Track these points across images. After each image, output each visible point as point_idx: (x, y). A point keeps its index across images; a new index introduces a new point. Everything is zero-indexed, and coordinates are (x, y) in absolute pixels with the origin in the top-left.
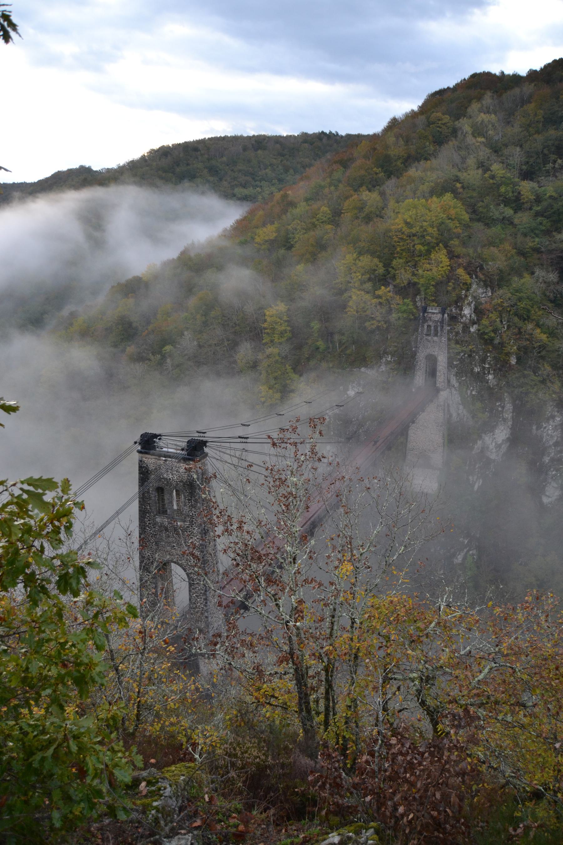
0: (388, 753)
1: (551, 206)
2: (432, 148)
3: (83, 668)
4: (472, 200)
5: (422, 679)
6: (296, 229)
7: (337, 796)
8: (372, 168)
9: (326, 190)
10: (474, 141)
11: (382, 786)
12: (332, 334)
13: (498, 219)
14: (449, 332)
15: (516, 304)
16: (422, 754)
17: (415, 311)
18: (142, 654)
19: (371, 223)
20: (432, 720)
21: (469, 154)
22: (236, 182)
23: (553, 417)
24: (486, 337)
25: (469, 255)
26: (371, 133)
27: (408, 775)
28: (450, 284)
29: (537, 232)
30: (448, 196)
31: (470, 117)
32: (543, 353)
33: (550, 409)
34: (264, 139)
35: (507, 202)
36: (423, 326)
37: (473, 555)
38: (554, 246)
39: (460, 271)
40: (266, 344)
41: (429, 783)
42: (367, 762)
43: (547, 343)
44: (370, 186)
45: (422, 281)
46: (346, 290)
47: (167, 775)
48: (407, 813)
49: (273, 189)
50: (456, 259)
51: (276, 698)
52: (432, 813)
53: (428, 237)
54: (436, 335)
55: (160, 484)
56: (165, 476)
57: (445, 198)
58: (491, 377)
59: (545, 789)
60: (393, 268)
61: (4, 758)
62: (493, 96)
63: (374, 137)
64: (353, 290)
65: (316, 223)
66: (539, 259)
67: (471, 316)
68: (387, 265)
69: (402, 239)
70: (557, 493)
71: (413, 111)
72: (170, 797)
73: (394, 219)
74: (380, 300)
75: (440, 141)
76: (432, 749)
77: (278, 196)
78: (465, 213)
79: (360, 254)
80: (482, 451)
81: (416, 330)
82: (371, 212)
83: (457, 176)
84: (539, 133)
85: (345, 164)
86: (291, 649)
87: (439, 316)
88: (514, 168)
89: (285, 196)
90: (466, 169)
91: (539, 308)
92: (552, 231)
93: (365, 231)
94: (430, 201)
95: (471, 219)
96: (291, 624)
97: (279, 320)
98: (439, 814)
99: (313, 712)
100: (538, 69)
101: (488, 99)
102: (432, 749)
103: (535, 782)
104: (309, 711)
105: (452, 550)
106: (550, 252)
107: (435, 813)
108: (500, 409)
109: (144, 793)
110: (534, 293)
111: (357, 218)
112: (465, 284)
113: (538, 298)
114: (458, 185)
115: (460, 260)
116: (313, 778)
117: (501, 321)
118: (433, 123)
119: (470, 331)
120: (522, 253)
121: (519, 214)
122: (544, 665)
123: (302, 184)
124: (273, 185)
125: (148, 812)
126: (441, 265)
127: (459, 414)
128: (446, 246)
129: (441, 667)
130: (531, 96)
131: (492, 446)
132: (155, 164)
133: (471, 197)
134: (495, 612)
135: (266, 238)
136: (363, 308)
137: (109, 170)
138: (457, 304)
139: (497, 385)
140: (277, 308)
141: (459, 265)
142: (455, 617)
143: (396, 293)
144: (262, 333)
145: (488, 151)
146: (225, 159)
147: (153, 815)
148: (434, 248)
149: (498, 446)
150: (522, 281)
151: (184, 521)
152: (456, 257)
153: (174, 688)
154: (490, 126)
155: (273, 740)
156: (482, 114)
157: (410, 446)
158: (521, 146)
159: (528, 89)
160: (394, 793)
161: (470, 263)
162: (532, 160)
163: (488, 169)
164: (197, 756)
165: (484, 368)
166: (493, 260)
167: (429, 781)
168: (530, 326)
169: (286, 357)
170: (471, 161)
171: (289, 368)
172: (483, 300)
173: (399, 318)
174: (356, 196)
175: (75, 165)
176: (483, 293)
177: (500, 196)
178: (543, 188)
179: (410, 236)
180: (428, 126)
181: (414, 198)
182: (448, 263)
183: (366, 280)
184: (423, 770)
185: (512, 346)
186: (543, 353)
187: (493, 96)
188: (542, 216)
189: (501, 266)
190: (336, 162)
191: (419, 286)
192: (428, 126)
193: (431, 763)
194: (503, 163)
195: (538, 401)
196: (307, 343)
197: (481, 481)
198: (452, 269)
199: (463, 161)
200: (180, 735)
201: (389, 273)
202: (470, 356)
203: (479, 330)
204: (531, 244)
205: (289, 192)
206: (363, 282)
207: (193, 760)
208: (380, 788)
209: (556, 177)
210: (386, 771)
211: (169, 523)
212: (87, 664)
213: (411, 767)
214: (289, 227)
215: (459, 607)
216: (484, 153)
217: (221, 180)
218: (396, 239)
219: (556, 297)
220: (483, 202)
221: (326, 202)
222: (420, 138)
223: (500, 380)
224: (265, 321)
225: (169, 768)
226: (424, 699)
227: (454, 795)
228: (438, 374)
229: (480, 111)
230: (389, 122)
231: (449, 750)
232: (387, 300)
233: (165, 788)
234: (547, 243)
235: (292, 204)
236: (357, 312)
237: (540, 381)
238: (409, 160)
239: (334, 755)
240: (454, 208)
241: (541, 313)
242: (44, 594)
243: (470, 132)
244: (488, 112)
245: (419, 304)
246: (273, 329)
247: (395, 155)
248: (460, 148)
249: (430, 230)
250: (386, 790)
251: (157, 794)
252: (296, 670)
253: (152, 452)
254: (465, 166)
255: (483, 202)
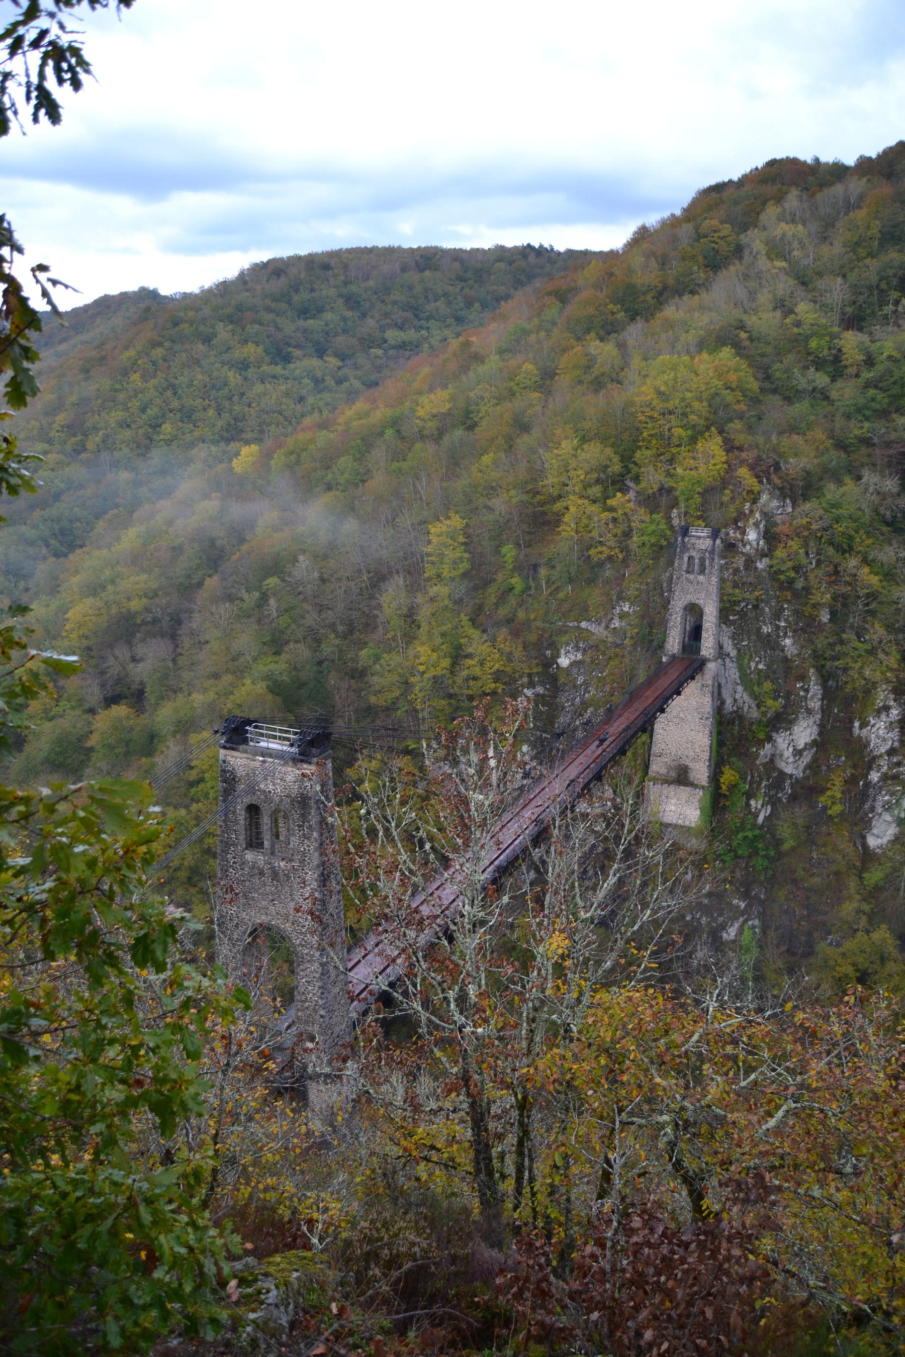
0: (627, 1242)
1: (890, 372)
2: (702, 275)
3: (168, 1087)
4: (765, 360)
5: (677, 1125)
6: (482, 398)
7: (542, 1311)
8: (606, 305)
9: (532, 338)
10: (769, 265)
11: (617, 1295)
12: (535, 567)
13: (804, 391)
14: (722, 568)
15: (831, 527)
16: (686, 1245)
17: (669, 533)
18: (224, 1072)
19: (603, 392)
20: (691, 1193)
21: (761, 286)
22: (388, 321)
23: (887, 708)
24: (782, 577)
25: (757, 446)
26: (606, 249)
27: (663, 1279)
28: (727, 492)
29: (867, 412)
30: (726, 352)
31: (765, 229)
32: (873, 606)
33: (882, 695)
34: (436, 254)
35: (819, 364)
36: (681, 558)
37: (753, 927)
38: (893, 436)
39: (743, 472)
40: (429, 579)
41: (696, 1293)
42: (593, 1256)
43: (880, 590)
44: (602, 333)
45: (681, 486)
46: (560, 497)
47: (272, 1269)
48: (658, 1341)
49: (447, 332)
50: (736, 452)
51: (438, 1150)
52: (698, 1341)
53: (692, 417)
54: (702, 571)
55: (253, 800)
56: (262, 786)
57: (721, 355)
58: (788, 642)
59: (874, 1310)
60: (636, 464)
61: (30, 1233)
62: (801, 196)
63: (612, 254)
64: (571, 497)
65: (515, 388)
66: (869, 455)
67: (758, 544)
68: (627, 458)
69: (651, 417)
70: (892, 831)
71: (673, 215)
72: (277, 1306)
73: (639, 387)
74: (614, 514)
75: (715, 264)
76: (702, 1237)
77: (454, 344)
78: (752, 379)
79: (584, 440)
80: (772, 761)
81: (671, 563)
82: (603, 374)
83: (741, 321)
84: (873, 257)
85: (562, 297)
86: (466, 1071)
87: (708, 542)
88: (832, 310)
89: (467, 344)
90: (755, 310)
91: (867, 533)
92: (890, 412)
93: (593, 405)
94: (697, 359)
95: (762, 390)
96: (468, 1030)
97: (450, 542)
98: (709, 1344)
99: (497, 1175)
100: (874, 156)
101: (793, 200)
102: (702, 1237)
103: (859, 1297)
104: (490, 1173)
105: (721, 919)
106: (888, 444)
107: (703, 1343)
108: (802, 693)
109: (234, 1298)
110: (860, 509)
111: (580, 382)
112: (751, 492)
113: (867, 518)
114: (743, 335)
115: (744, 455)
116: (503, 1280)
117: (807, 554)
118: (705, 236)
119: (756, 568)
120: (841, 445)
121: (839, 384)
122: (874, 1108)
123: (493, 326)
124: (447, 326)
125: (240, 1329)
126: (712, 462)
127: (735, 700)
128: (721, 432)
129: (709, 1106)
130: (861, 197)
131: (788, 753)
132: (259, 287)
133: (763, 355)
134: (796, 1019)
135: (435, 411)
136: (587, 526)
137: (185, 296)
138: (736, 524)
139: (799, 655)
140: (448, 522)
141: (742, 462)
142: (730, 1025)
143: (640, 504)
144: (423, 561)
145: (792, 282)
146: (371, 283)
147: (248, 1334)
148: (702, 433)
149: (798, 753)
150: (842, 490)
151: (291, 860)
152: (737, 448)
153: (274, 1128)
154: (796, 243)
155: (434, 1217)
156: (783, 225)
157: (655, 749)
158: (844, 276)
159: (856, 186)
160: (637, 1309)
161: (759, 459)
162: (861, 298)
163: (791, 312)
164: (315, 1241)
165: (778, 627)
166: (796, 455)
167: (695, 1289)
168: (853, 562)
169: (459, 602)
170: (764, 298)
171: (464, 619)
172: (778, 519)
173: (644, 544)
174: (580, 348)
175: (132, 286)
176: (779, 507)
177: (809, 354)
178: (878, 344)
179: (664, 414)
180: (698, 240)
181: (672, 353)
182: (724, 459)
183: (592, 481)
184: (685, 1272)
185: (823, 593)
186: (873, 606)
187: (801, 196)
188: (876, 387)
189: (808, 467)
190: (549, 293)
191: (677, 493)
192: (698, 240)
193: (701, 1260)
194: (815, 302)
195: (863, 682)
196: (495, 580)
197: (769, 807)
198: (730, 468)
199: (751, 295)
200: (282, 1207)
201: (629, 472)
202: (756, 607)
203: (771, 567)
204: (857, 432)
205: (474, 339)
206: (586, 486)
207: (307, 1246)
208: (614, 1300)
209: (899, 326)
210: (624, 1271)
211: (267, 862)
212: (175, 1082)
213: (668, 1264)
214: (472, 395)
215: (738, 1011)
216: (785, 285)
217: (364, 315)
218: (643, 418)
219: (894, 517)
220: (782, 362)
221: (531, 355)
222: (683, 259)
223: (803, 647)
224: (429, 542)
225: (271, 1259)
226: (679, 1157)
227: (735, 1312)
228: (704, 635)
229: (781, 218)
230: (636, 233)
231: (729, 1240)
232: (626, 514)
233: (268, 1292)
234: (883, 430)
235: (478, 358)
236: (577, 532)
237: (867, 651)
238: (664, 294)
239: (538, 1244)
240: (736, 370)
241: (870, 541)
242: (112, 966)
243: (764, 252)
244: (793, 221)
245: (676, 522)
246: (442, 555)
247: (643, 285)
248: (746, 277)
249: (696, 405)
250: (623, 1302)
251: (255, 1300)
252: (473, 1105)
253: (241, 747)
254: (754, 305)
255: (782, 362)
